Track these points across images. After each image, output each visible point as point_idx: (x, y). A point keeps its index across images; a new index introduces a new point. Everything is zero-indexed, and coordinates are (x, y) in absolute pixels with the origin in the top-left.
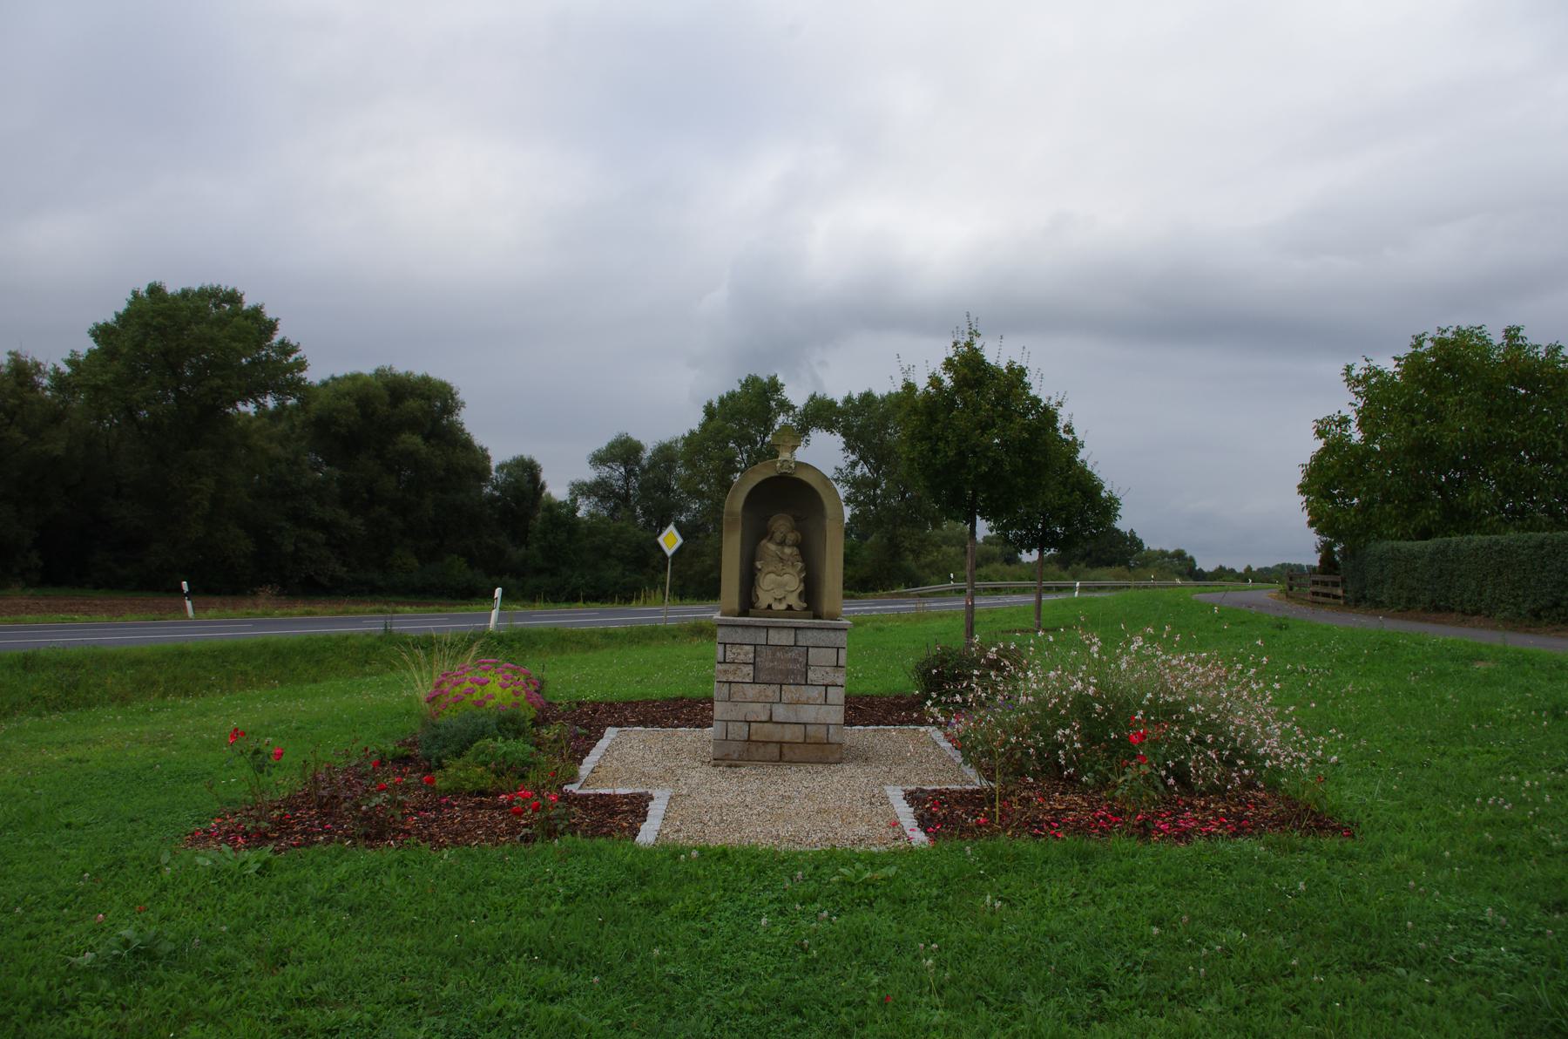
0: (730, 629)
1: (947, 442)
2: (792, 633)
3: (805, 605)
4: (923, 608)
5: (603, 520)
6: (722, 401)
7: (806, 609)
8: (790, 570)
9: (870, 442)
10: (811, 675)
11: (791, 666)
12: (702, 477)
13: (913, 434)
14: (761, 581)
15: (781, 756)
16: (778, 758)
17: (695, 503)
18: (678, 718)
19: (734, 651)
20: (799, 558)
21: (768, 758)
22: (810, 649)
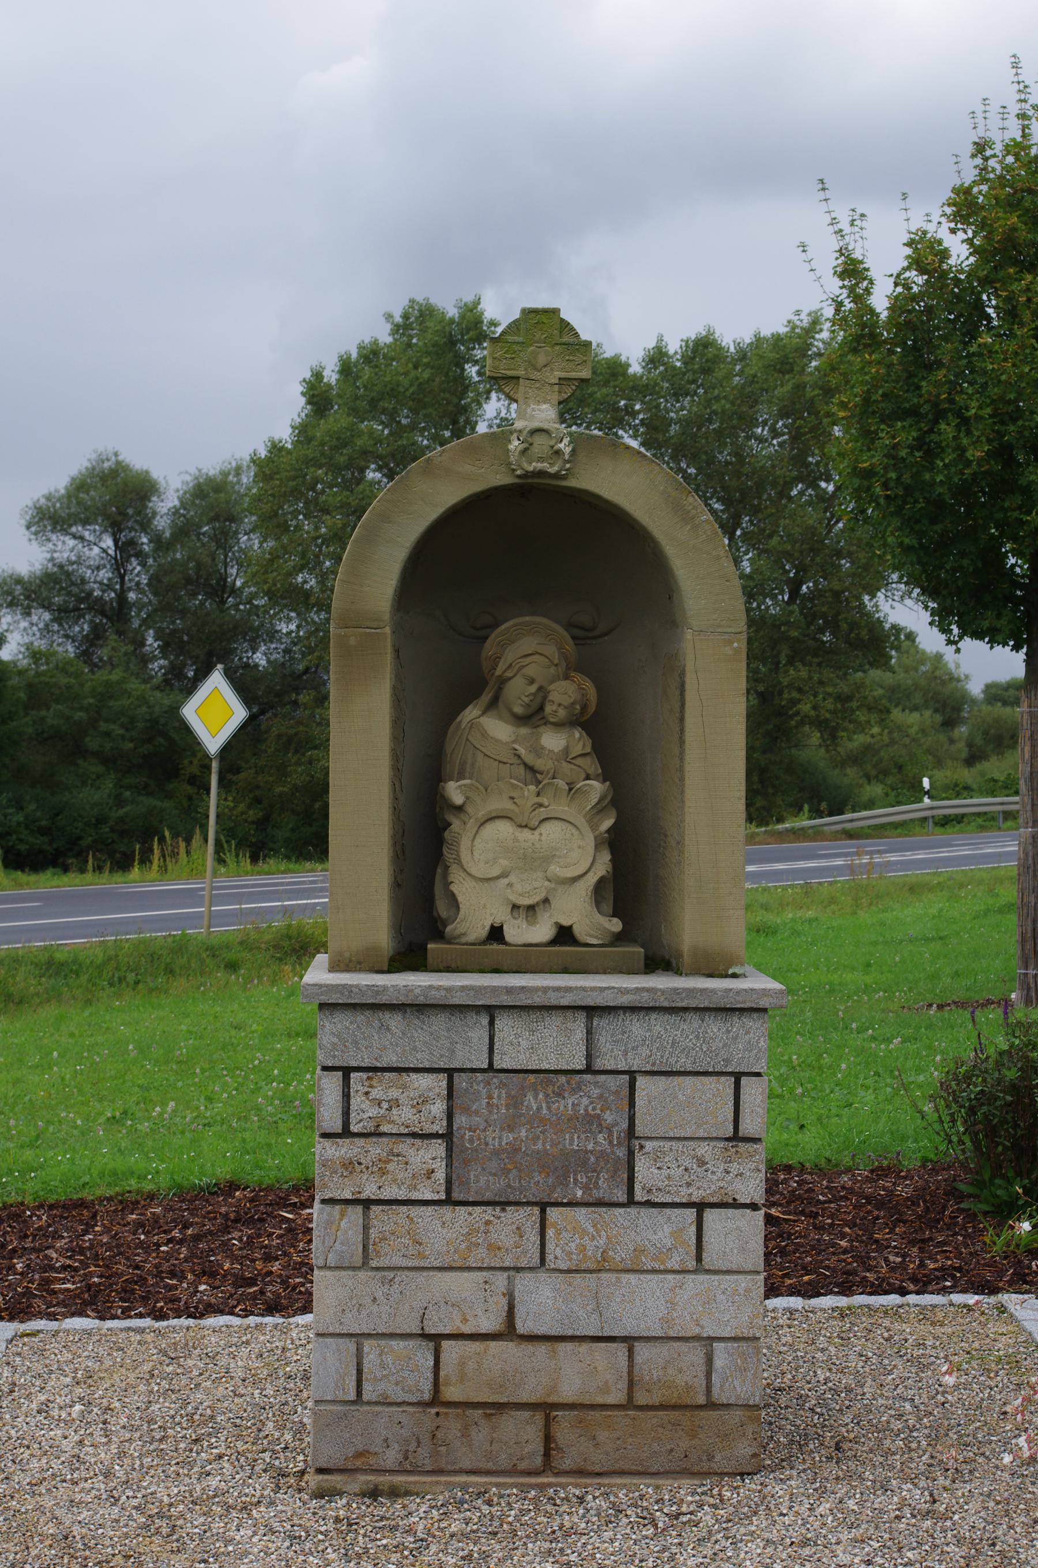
0: (361, 1018)
1: (965, 422)
2: (578, 1027)
3: (616, 925)
4: (870, 867)
5: (64, 667)
6: (346, 368)
7: (618, 939)
8: (561, 807)
9: (711, 461)
10: (644, 1170)
11: (574, 1142)
12: (303, 555)
13: (867, 401)
14: (465, 843)
15: (547, 1454)
16: (539, 1461)
17: (289, 620)
18: (209, 1273)
19: (375, 1093)
20: (591, 765)
21: (504, 1461)
22: (641, 1081)
